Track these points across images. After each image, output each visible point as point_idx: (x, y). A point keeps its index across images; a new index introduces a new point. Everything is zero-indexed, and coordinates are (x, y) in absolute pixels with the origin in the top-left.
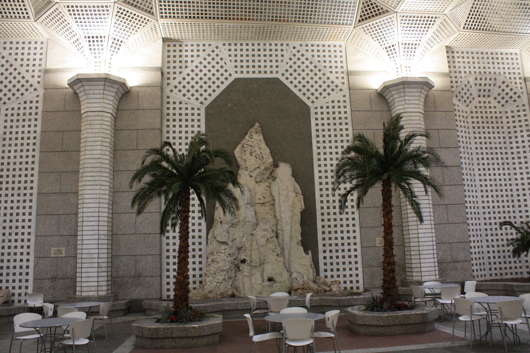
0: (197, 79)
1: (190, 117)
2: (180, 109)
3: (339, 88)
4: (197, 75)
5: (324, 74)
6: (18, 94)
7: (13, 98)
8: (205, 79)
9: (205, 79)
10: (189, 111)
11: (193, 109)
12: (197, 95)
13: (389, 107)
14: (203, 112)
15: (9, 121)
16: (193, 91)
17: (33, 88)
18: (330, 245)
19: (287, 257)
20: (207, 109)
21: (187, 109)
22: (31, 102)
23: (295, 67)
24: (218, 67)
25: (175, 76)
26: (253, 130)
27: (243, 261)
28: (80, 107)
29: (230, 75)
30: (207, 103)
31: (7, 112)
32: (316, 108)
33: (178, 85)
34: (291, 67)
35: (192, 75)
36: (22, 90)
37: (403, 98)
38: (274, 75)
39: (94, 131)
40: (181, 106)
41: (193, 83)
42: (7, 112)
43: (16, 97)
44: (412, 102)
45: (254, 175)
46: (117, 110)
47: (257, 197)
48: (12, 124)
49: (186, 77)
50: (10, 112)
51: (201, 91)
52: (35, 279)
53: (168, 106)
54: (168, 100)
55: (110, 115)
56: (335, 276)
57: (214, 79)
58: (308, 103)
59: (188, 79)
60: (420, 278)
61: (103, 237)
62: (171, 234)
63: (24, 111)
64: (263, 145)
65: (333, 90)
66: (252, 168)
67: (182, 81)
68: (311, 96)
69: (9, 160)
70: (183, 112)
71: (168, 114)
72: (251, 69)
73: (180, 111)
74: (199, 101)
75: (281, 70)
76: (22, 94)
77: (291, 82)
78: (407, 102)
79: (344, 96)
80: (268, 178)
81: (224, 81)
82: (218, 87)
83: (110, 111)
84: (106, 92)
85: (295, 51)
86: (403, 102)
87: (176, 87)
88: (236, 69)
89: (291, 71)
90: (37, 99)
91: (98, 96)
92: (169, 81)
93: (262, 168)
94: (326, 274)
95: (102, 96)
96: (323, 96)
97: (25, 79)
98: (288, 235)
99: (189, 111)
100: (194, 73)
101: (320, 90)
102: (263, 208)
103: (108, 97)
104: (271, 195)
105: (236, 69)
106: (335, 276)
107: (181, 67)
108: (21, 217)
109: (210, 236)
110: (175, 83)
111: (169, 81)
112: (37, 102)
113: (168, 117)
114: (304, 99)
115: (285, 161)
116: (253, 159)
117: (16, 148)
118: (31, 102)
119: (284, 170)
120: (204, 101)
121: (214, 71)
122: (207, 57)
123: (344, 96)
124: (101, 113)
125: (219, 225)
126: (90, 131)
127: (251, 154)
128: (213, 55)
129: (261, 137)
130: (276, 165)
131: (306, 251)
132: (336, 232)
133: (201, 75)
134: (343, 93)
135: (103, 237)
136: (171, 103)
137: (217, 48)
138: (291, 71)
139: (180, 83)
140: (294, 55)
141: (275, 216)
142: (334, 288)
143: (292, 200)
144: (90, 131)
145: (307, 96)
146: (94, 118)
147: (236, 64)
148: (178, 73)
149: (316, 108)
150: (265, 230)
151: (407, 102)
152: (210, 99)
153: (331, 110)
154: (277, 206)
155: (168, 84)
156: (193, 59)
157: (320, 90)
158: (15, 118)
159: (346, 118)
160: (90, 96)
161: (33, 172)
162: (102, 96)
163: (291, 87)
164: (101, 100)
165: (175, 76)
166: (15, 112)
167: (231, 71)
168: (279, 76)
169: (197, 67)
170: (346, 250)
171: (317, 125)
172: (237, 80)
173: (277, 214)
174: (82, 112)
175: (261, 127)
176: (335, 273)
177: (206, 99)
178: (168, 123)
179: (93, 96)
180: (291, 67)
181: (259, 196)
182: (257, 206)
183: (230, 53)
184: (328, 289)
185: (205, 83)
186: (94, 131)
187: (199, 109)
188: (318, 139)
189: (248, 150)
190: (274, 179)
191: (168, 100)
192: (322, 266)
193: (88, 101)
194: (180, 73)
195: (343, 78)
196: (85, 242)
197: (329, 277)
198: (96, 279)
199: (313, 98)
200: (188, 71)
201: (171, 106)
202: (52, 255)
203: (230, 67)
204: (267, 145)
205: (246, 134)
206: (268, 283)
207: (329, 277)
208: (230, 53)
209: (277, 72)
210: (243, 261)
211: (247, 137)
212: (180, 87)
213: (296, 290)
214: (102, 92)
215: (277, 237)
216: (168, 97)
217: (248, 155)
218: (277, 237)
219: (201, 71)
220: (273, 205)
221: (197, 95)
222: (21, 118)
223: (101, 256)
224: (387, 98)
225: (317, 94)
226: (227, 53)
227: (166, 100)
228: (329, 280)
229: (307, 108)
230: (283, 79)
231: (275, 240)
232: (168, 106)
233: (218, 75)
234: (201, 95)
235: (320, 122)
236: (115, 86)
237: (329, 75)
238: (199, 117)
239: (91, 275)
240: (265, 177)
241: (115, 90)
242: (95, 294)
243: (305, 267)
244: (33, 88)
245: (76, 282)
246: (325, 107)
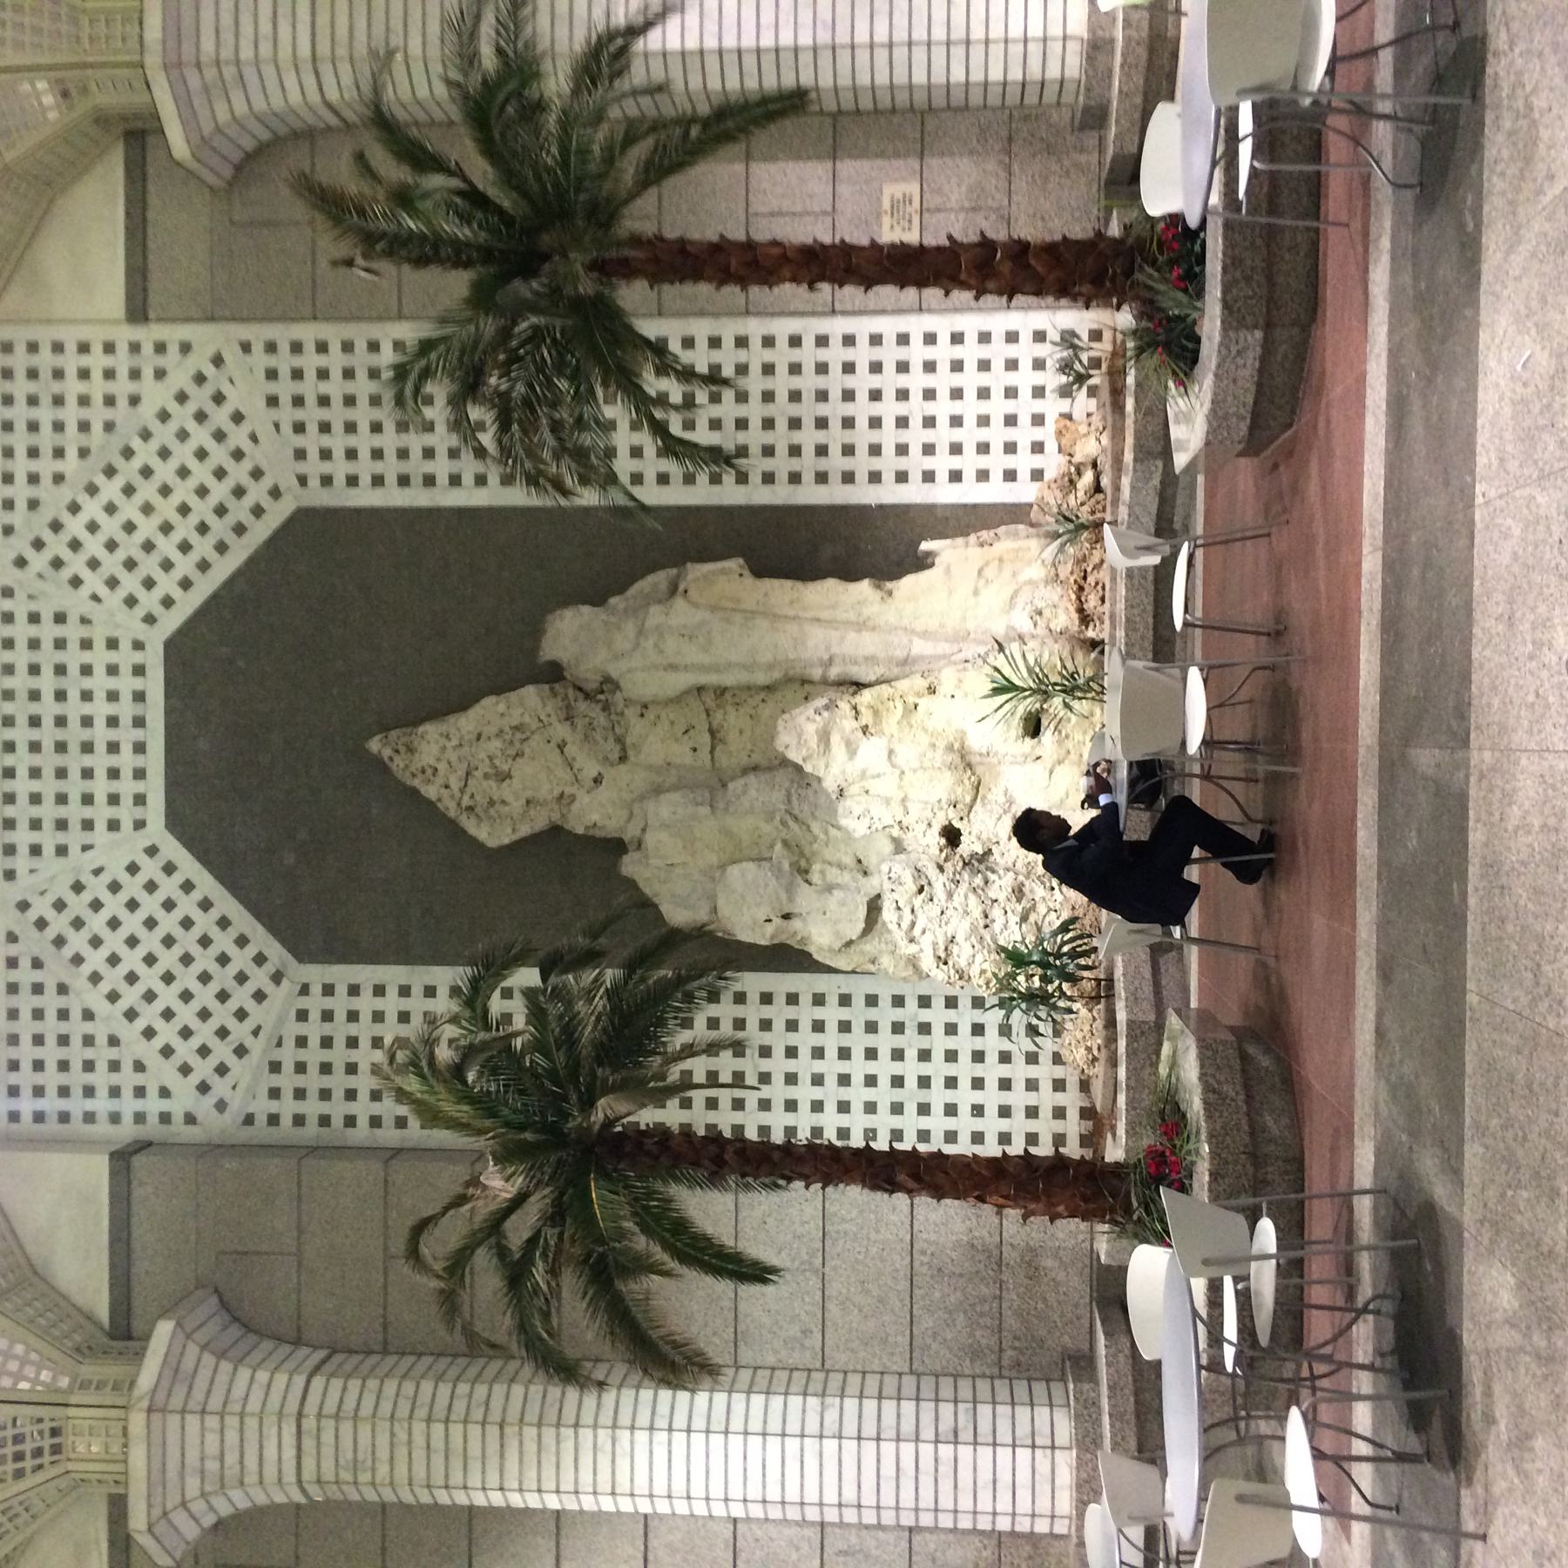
0: (168, 996)
1: (340, 1029)
2: (301, 1068)
3: (209, 370)
4: (150, 996)
5: (146, 435)
8: (168, 959)
9: (168, 959)
10: (314, 1030)
11: (302, 1016)
12: (241, 997)
13: (296, 135)
14: (316, 974)
16: (223, 1015)
19: (943, 648)
20: (303, 954)
21: (302, 1042)
23: (112, 564)
24: (114, 905)
25: (153, 1092)
26: (398, 765)
27: (952, 836)
28: (274, 1508)
29: (152, 851)
30: (276, 952)
32: (303, 480)
33: (194, 1079)
34: (112, 583)
35: (150, 1015)
37: (250, 74)
38: (154, 658)
39: (383, 1453)
40: (288, 1067)
41: (186, 1014)
44: (266, 28)
45: (591, 769)
46: (297, 1342)
47: (688, 759)
49: (158, 1043)
51: (224, 978)
53: (286, 1121)
54: (261, 1120)
55: (318, 1382)
56: (1038, 434)
57: (169, 923)
58: (277, 514)
59: (167, 1033)
60: (1074, 48)
61: (832, 1416)
64: (467, 722)
65: (219, 398)
66: (563, 774)
67: (177, 1060)
68: (248, 501)
70: (314, 1055)
71: (325, 1121)
72: (126, 760)
73: (313, 1069)
74: (269, 988)
75: (130, 625)
77: (186, 584)
78: (265, 49)
79: (246, 347)
80: (606, 707)
81: (178, 878)
82: (206, 905)
83: (300, 1381)
84: (215, 1403)
85: (38, 562)
86: (269, 71)
87: (204, 1088)
88: (126, 825)
89: (130, 583)
90: (257, 348)
91: (232, 1436)
92: (178, 1117)
93: (561, 731)
94: (1024, 474)
95: (232, 1422)
96: (246, 445)
99: (314, 1030)
101: (219, 455)
102: (732, 736)
103: (238, 1392)
104: (678, 700)
105: (126, 825)
106: (1038, 434)
107: (114, 1066)
109: (841, 963)
110: (183, 1090)
111: (178, 1117)
113: (338, 1122)
114: (260, 532)
115: (536, 631)
116: (524, 771)
119: (570, 634)
120: (270, 968)
121: (132, 923)
122: (68, 952)
123: (246, 347)
124: (309, 1423)
125: (796, 924)
126: (383, 1470)
127: (504, 777)
128: (59, 924)
129: (430, 729)
130: (553, 674)
131: (923, 563)
132: (168, 978)
133: (150, 978)
134: (232, 355)
135: (832, 1416)
136: (274, 1106)
137: (24, 906)
138: (130, 583)
139: (185, 1070)
140: (57, 563)
141: (769, 688)
142: (1088, 448)
143: (701, 615)
144: (383, 1470)
145: (246, 517)
146: (328, 1452)
147: (101, 826)
148: (139, 1079)
149: (303, 480)
150: (825, 737)
151: (265, 49)
152: (262, 940)
153: (312, 414)
154: (729, 679)
155: (190, 1119)
156: (76, 1014)
157: (219, 455)
159: (348, 347)
160: (232, 1470)
162: (232, 1422)
163: (205, 587)
164: (252, 1423)
165: (153, 1092)
167: (130, 846)
168: (156, 640)
169: (113, 997)
170: (929, 381)
171: (378, 481)
172: (175, 822)
173: (761, 678)
174: (299, 1498)
175: (385, 729)
176: (1024, 435)
177: (260, 959)
178: (363, 1122)
179: (231, 1458)
180: (112, 583)
181: (680, 753)
182: (723, 760)
183: (49, 850)
184: (1088, 477)
185: (187, 960)
186: (383, 1453)
187: (305, 990)
188: (442, 479)
189: (483, 788)
190: (609, 684)
191: (261, 1120)
192: (995, 492)
193: (251, 1478)
194: (139, 1067)
195: (160, 348)
196: (850, 1495)
197: (1037, 461)
198: (1004, 1454)
199: (257, 493)
200: (130, 1033)
201: (287, 1107)
203: (113, 852)
204: (463, 706)
205: (415, 792)
206: (1047, 736)
207: (1037, 461)
208: (49, 850)
209: (138, 646)
210: (952, 836)
211: (431, 792)
212: (203, 1069)
213: (1085, 619)
214: (212, 1422)
215: (859, 686)
216: (249, 1120)
217: (505, 791)
218: (859, 686)
219: (132, 978)
220: (721, 692)
221: (241, 997)
223: (908, 1427)
224: (249, 144)
225: (239, 473)
226: (49, 863)
227: (261, 1132)
228: (1053, 464)
229: (302, 516)
230: (172, 622)
231: (866, 696)
232: (286, 1121)
233: (151, 905)
234: (241, 978)
235: (365, 467)
236: (189, 1363)
237: (147, 411)
238: (341, 990)
239: (985, 1475)
240: (602, 720)
241: (208, 1359)
242: (1066, 1462)
243: (990, 572)
245: (1013, 1534)
246: (300, 441)
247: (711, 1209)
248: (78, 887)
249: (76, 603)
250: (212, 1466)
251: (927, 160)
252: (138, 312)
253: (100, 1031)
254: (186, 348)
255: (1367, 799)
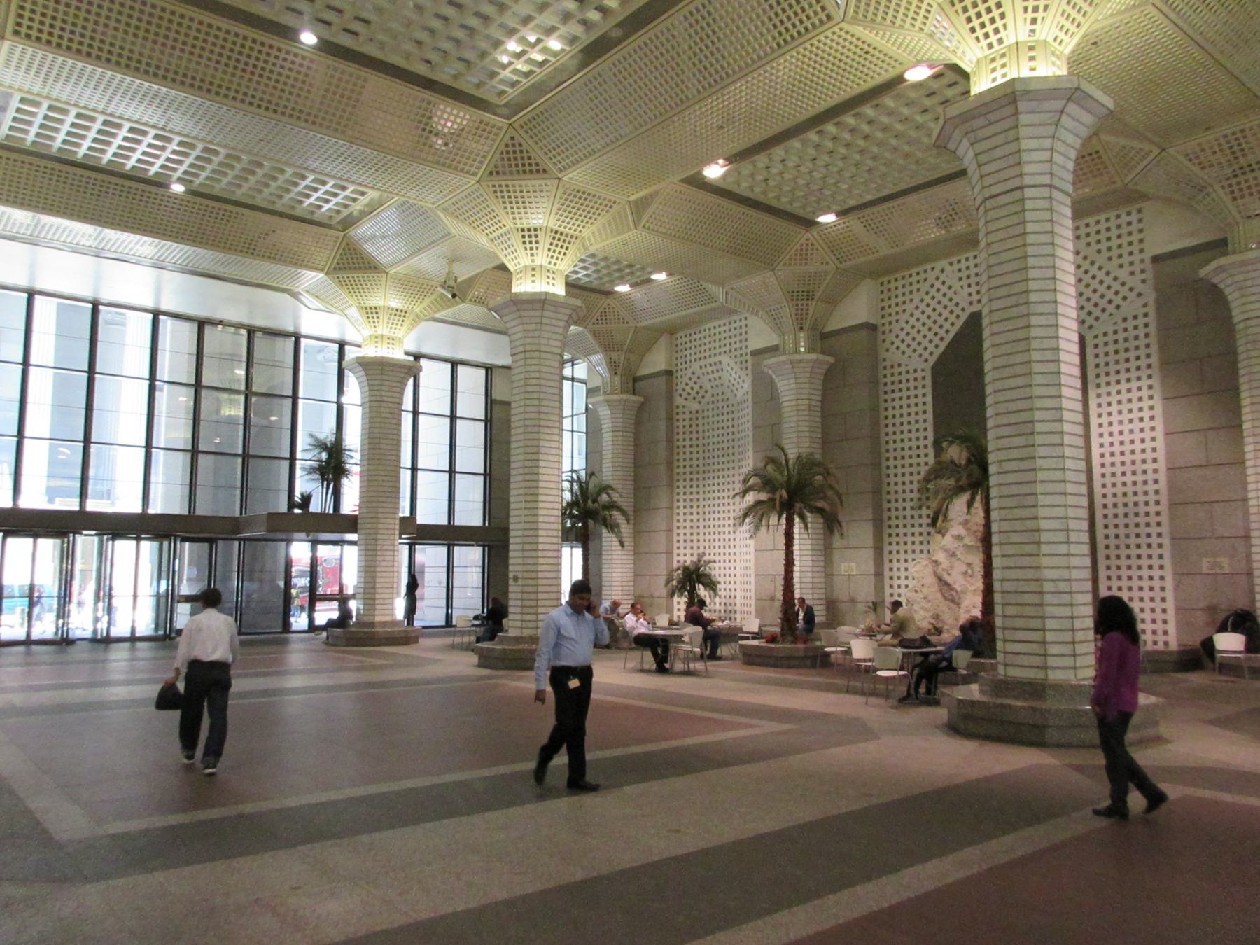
6: (1111, 308)
7: (1104, 316)
15: (1102, 355)
17: (1136, 292)
18: (1137, 525)
22: (1135, 317)
31: (1096, 341)
36: (1118, 300)
42: (1096, 341)
43: (1107, 313)
48: (1107, 359)
50: (1101, 340)
52: (1178, 610)
62: (957, 530)
63: (1125, 335)
69: (1111, 419)
76: (1118, 307)
90: (1145, 310)
97: (1130, 318)
98: (305, 582)
100: (1120, 573)
108: (906, 428)
112: (1146, 315)
117: (1119, 397)
118: (1135, 317)
134: (1142, 301)
158: (1111, 348)
161: (1153, 434)
166: (1111, 338)
202: (1205, 571)
222: (1121, 346)
244: (1136, 292)
247: (978, 504)
248: (950, 288)
249: (957, 286)
250: (1249, 283)
251: (28, 583)
252: (1156, 259)
253: (1116, 262)
254: (1144, 281)
255: (1226, 797)
